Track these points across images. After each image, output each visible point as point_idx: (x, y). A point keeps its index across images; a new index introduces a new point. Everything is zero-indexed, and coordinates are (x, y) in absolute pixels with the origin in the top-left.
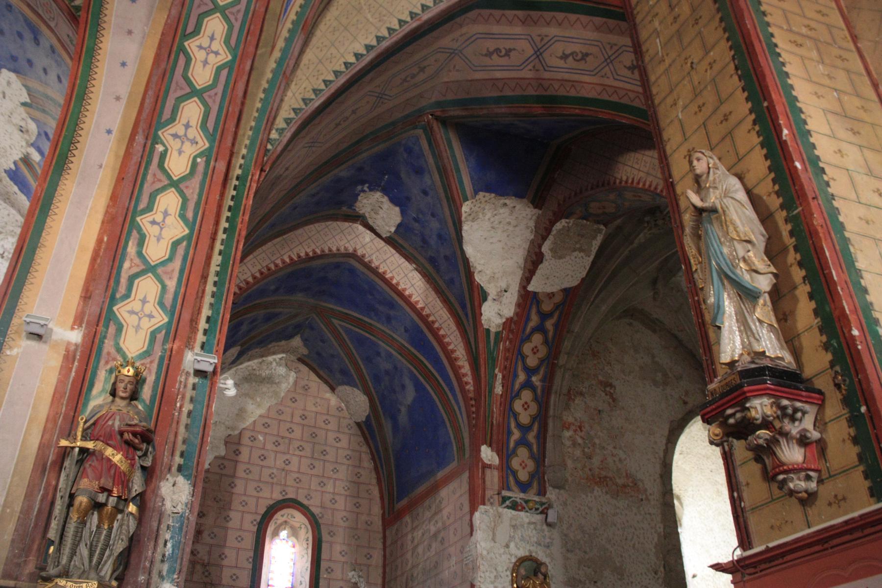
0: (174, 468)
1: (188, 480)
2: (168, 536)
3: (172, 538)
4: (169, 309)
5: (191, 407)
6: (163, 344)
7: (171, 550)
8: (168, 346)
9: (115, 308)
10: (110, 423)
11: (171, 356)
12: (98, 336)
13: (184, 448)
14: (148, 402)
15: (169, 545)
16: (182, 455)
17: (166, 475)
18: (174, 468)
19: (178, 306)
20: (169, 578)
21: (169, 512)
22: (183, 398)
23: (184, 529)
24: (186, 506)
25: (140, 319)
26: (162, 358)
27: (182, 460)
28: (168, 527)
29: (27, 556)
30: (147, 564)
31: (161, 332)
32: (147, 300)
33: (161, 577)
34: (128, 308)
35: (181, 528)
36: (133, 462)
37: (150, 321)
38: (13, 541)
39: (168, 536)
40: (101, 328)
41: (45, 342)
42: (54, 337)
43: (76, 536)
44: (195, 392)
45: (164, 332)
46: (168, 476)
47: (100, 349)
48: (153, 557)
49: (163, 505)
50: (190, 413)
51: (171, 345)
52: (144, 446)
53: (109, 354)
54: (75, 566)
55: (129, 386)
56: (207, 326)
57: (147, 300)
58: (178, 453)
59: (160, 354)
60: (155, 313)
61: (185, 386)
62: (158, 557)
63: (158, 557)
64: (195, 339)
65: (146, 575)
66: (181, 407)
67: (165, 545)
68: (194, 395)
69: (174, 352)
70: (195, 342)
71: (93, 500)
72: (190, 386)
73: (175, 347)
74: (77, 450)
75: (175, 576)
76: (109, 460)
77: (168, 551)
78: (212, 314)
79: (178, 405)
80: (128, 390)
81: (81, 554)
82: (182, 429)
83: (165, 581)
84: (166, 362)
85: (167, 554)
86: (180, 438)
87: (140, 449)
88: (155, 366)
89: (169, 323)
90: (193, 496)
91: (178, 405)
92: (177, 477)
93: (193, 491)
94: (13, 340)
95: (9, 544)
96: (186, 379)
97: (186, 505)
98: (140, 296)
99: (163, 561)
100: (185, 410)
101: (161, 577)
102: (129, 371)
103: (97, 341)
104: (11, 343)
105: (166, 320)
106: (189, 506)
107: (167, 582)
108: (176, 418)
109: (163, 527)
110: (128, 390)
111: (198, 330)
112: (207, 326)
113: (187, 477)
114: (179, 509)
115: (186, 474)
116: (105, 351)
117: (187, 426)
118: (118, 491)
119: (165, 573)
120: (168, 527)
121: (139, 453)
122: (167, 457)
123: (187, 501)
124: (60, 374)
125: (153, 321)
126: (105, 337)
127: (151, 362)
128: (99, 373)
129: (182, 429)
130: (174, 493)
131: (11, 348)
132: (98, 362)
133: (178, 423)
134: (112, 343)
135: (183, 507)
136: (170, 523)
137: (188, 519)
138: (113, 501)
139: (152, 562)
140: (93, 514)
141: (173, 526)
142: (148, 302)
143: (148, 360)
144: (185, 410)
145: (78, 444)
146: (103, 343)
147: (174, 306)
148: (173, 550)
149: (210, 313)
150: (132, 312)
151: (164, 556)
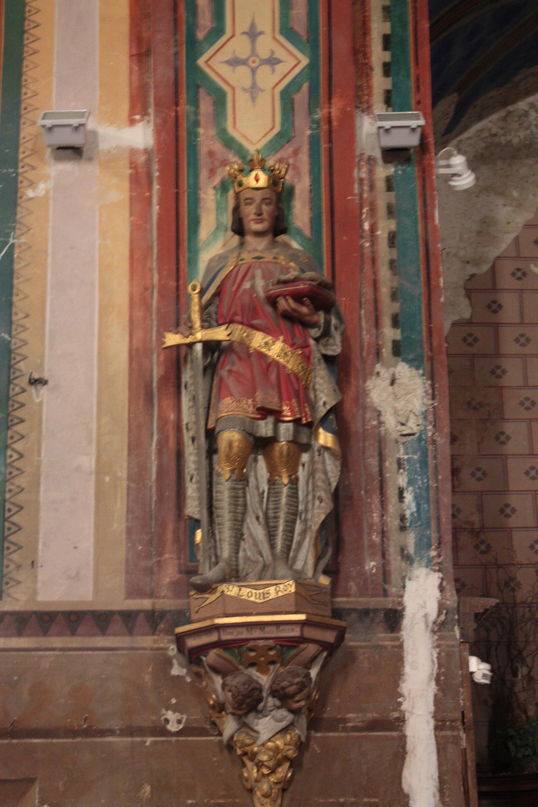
0: (387, 351)
1: (417, 368)
2: (402, 481)
3: (411, 482)
4: (305, 37)
5: (392, 226)
6: (311, 111)
7: (413, 505)
8: (319, 114)
9: (201, 62)
10: (247, 285)
11: (330, 132)
12: (184, 125)
13: (396, 307)
14: (307, 232)
15: (409, 497)
16: (396, 322)
17: (373, 366)
18: (387, 351)
19: (322, 29)
20: (421, 557)
21: (395, 435)
22: (373, 211)
23: (431, 462)
24: (425, 418)
25: (254, 71)
26: (314, 141)
27: (399, 331)
28: (400, 464)
29: (161, 555)
30: (376, 538)
31: (299, 89)
32: (259, 30)
33: (407, 558)
34: (226, 54)
35: (424, 462)
36: (306, 350)
37: (273, 71)
38: (129, 531)
39: (402, 481)
40: (185, 108)
41: (90, 160)
42: (103, 146)
43: (237, 505)
44: (393, 194)
45: (305, 87)
46: (378, 367)
47: (193, 148)
48: (383, 523)
49: (381, 423)
50: (392, 239)
51: (326, 111)
52: (321, 317)
53: (211, 154)
54: (247, 559)
55: (265, 208)
56: (387, 56)
57: (259, 30)
58: (386, 321)
59: (309, 132)
60: (280, 54)
61: (372, 187)
62: (394, 523)
63: (394, 523)
64: (369, 87)
65: (379, 557)
66: (373, 229)
67: (401, 497)
68: (393, 201)
69: (335, 123)
70: (370, 95)
71: (250, 434)
72: (381, 185)
73: (335, 111)
74: (199, 347)
75: (433, 553)
76: (262, 356)
77: (409, 508)
78: (392, 28)
79: (366, 226)
80: (265, 216)
81: (251, 534)
82: (384, 273)
83: (416, 564)
84: (324, 146)
85: (408, 513)
86: (385, 291)
87: (314, 325)
88: (304, 158)
89: (312, 66)
90: (433, 397)
91: (366, 226)
92: (395, 366)
93: (433, 386)
94: (33, 168)
95: (124, 536)
96: (371, 172)
97: (425, 416)
98: (243, 25)
99: (403, 528)
100: (382, 234)
101: (407, 558)
102: (257, 179)
103: (184, 134)
104: (30, 175)
105: (305, 61)
106: (431, 417)
107: (420, 566)
108: (367, 252)
109: (390, 464)
110: (265, 216)
111: (371, 69)
112: (387, 56)
113: (412, 362)
114: (413, 426)
115: (411, 356)
116: (203, 150)
117: (392, 264)
118: (291, 410)
119: (411, 550)
120: (400, 464)
121: (315, 332)
122: (368, 331)
123: (424, 409)
124: (131, 215)
125: (281, 69)
126: (197, 124)
127: (296, 152)
128: (202, 195)
129: (384, 273)
130: (396, 397)
131: (32, 184)
132: (196, 175)
133: (374, 261)
134: (212, 132)
135: (421, 421)
136: (401, 454)
137: (434, 442)
138: (287, 430)
139: (383, 534)
140: (256, 460)
141: (408, 460)
142: (261, 33)
143: (289, 150)
144: (382, 234)
145: (199, 336)
146: (196, 135)
147: (313, 30)
148: (418, 505)
149: (387, 28)
150: (235, 62)
151: (403, 518)
